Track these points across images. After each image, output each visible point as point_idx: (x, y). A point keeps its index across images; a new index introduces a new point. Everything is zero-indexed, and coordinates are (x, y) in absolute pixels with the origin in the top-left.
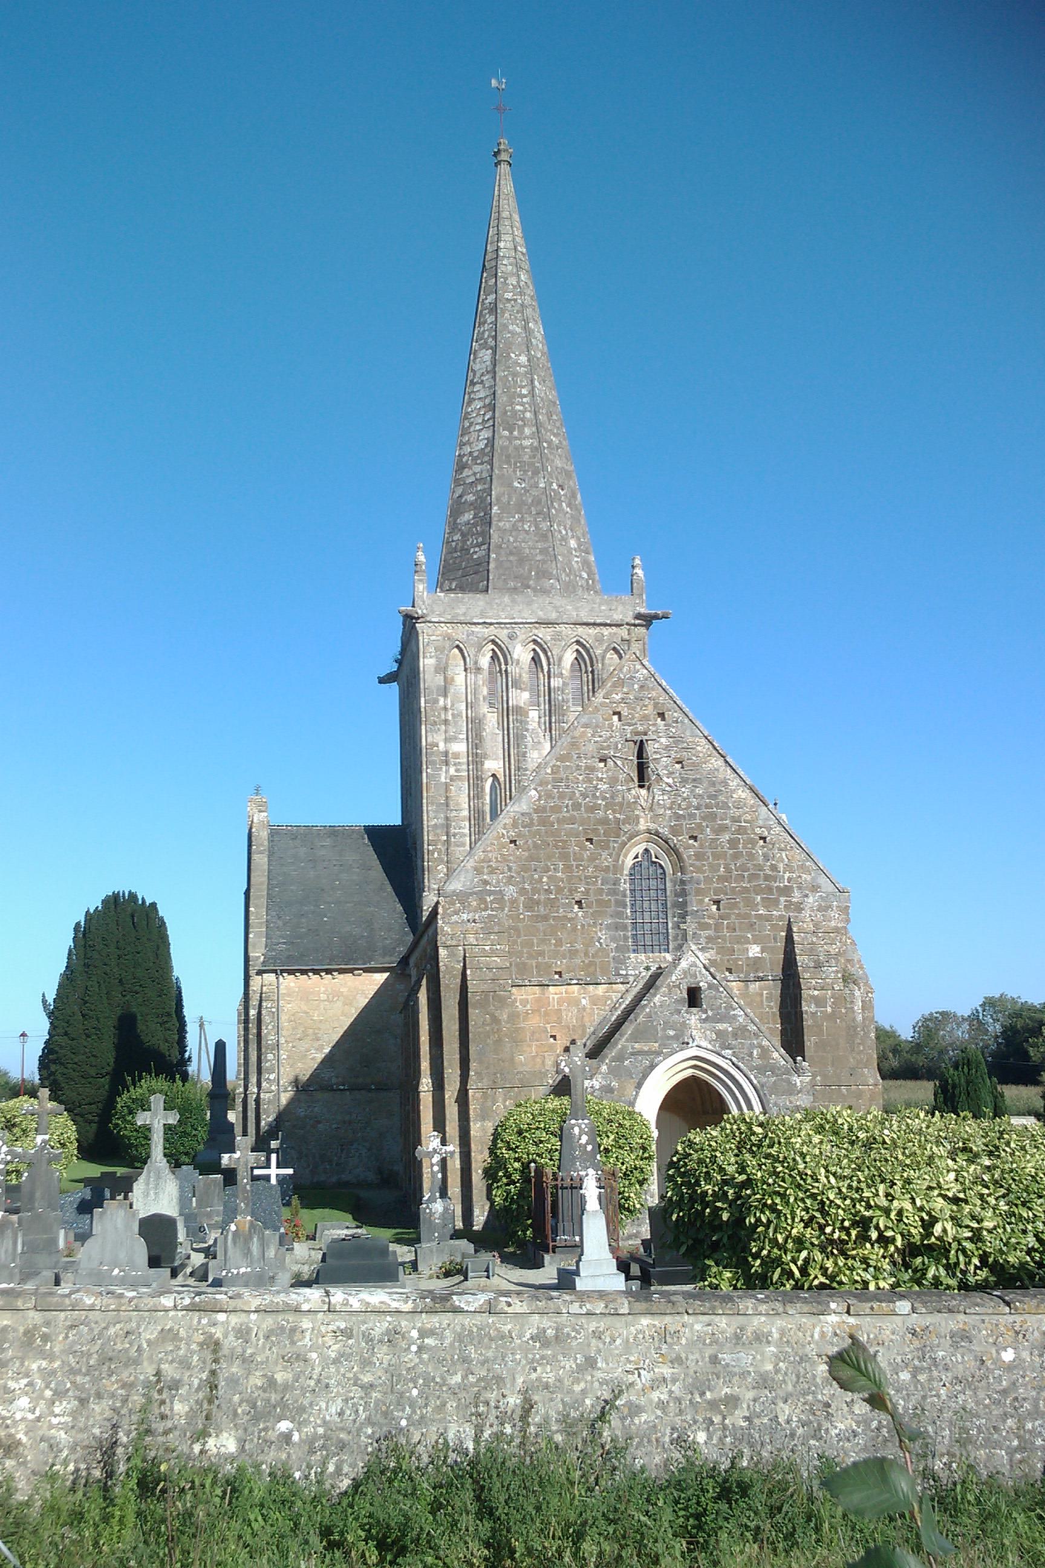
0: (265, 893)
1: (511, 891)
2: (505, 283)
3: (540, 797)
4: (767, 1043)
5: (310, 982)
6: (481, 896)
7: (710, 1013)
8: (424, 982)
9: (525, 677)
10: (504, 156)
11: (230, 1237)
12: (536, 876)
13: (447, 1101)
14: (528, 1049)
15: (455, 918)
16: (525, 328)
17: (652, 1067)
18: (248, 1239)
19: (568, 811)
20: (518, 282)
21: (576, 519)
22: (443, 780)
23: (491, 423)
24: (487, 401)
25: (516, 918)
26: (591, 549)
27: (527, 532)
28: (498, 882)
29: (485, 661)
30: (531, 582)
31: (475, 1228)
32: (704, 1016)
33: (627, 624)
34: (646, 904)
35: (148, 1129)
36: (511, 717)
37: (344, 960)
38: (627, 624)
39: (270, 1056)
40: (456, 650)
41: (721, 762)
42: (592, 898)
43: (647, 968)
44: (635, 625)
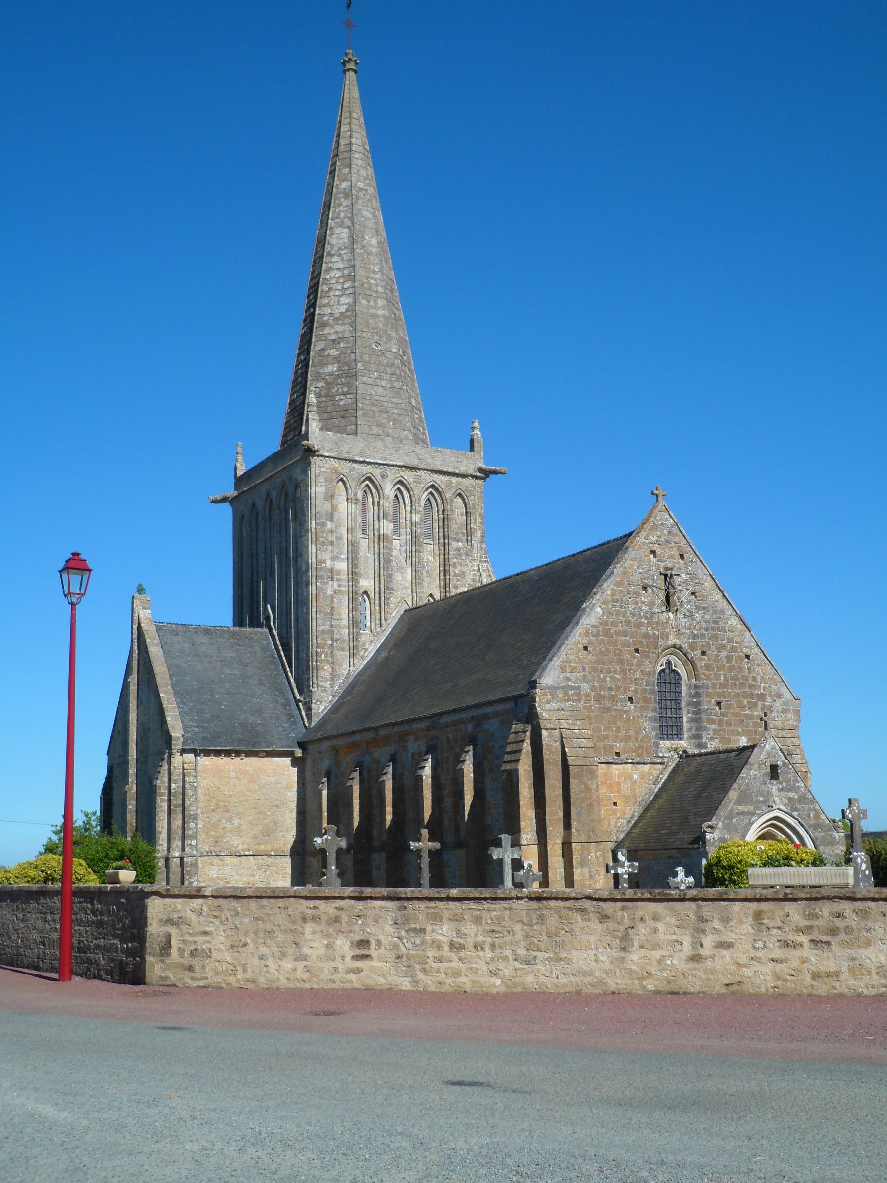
1: (585, 687)
3: (604, 613)
7: (784, 784)
15: (548, 706)
19: (622, 626)
24: (346, 272)
25: (588, 708)
28: (577, 679)
35: (500, 862)
36: (381, 543)
39: (192, 825)
41: (720, 595)
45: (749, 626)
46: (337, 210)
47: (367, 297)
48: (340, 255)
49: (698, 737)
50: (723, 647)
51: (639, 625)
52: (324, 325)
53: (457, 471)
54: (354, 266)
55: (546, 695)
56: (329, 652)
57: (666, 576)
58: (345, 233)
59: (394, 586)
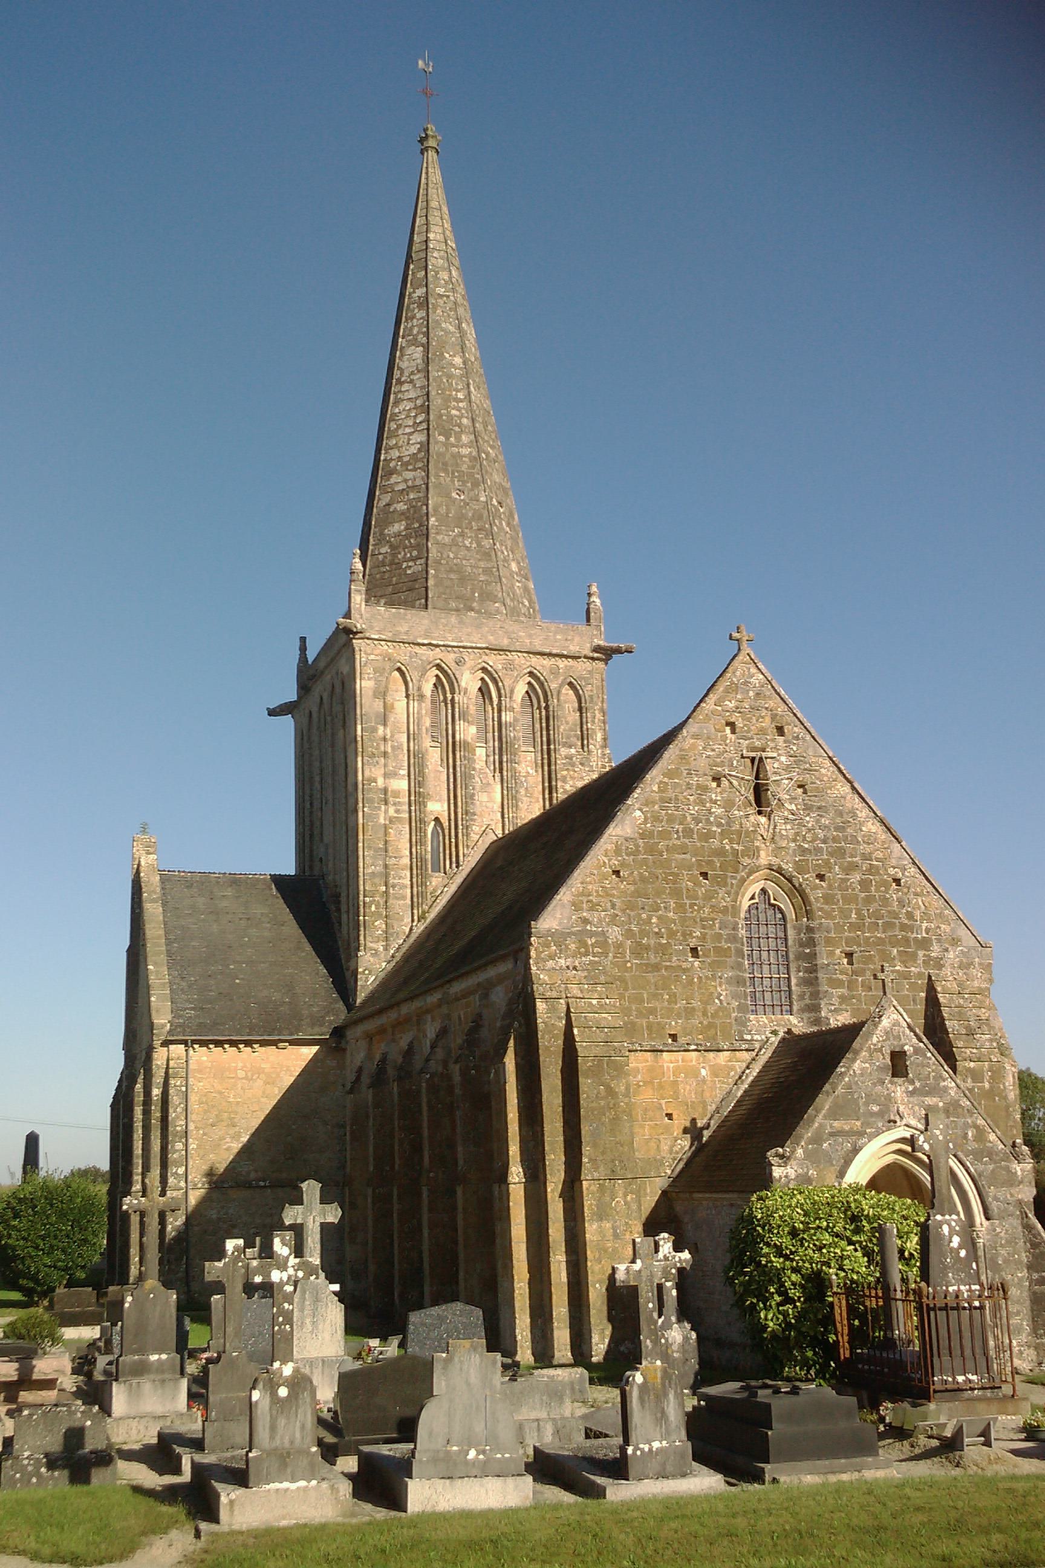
0: (164, 948)
2: (436, 277)
3: (646, 819)
4: (983, 1122)
5: (225, 1056)
6: (581, 937)
7: (918, 1084)
8: (511, 1043)
9: (472, 709)
10: (431, 143)
11: (635, 1394)
12: (644, 916)
13: (549, 1197)
14: (641, 1131)
15: (550, 964)
16: (459, 327)
17: (856, 1151)
18: (661, 1397)
19: (678, 838)
20: (451, 277)
21: (514, 539)
22: (382, 821)
23: (424, 425)
24: (419, 402)
25: (622, 966)
26: (530, 576)
27: (468, 549)
28: (600, 920)
29: (428, 688)
30: (475, 604)
31: (594, 1359)
32: (911, 1088)
33: (585, 657)
34: (765, 954)
37: (268, 1032)
38: (585, 657)
39: (179, 1146)
40: (396, 674)
41: (847, 788)
42: (710, 945)
43: (774, 1033)
44: (593, 659)
45: (899, 834)
46: (410, 325)
47: (447, 434)
48: (411, 381)
49: (814, 1008)
50: (853, 867)
51: (707, 836)
52: (391, 473)
53: (565, 653)
54: (428, 394)
55: (549, 947)
56: (382, 902)
57: (753, 760)
58: (417, 353)
59: (478, 810)
